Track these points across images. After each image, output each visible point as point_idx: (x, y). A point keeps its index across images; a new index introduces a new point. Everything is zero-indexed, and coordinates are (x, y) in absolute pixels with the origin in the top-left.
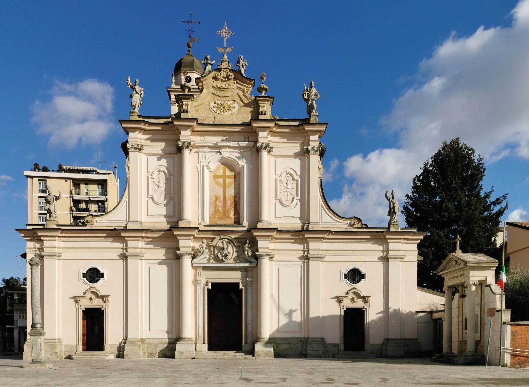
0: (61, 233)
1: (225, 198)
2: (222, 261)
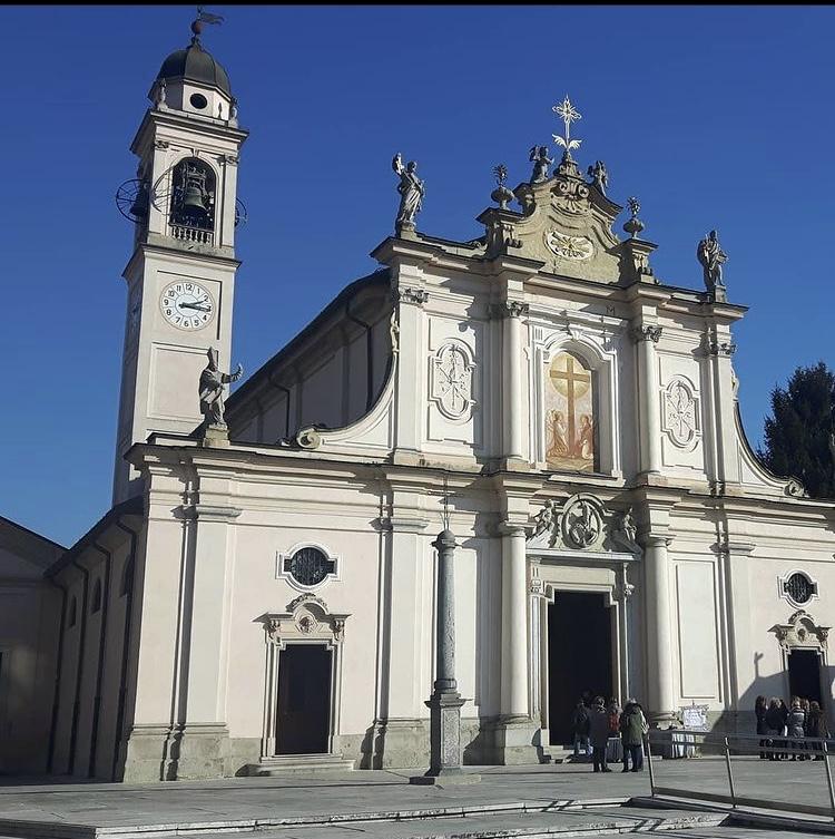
1: (571, 418)
2: (581, 546)
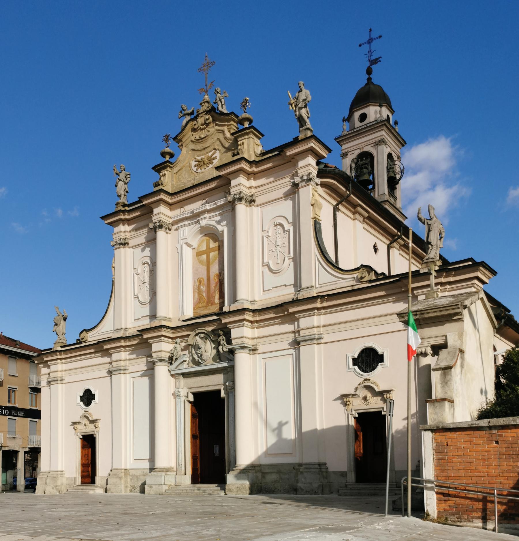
0: (125, 341)
